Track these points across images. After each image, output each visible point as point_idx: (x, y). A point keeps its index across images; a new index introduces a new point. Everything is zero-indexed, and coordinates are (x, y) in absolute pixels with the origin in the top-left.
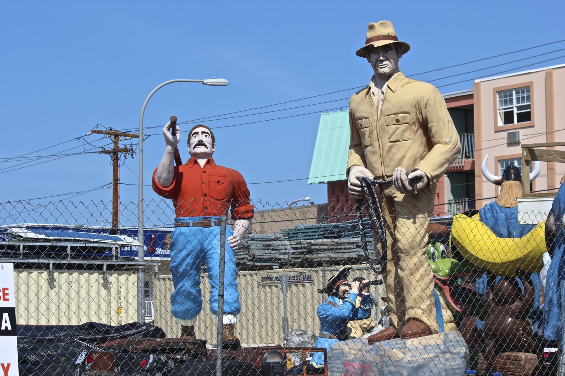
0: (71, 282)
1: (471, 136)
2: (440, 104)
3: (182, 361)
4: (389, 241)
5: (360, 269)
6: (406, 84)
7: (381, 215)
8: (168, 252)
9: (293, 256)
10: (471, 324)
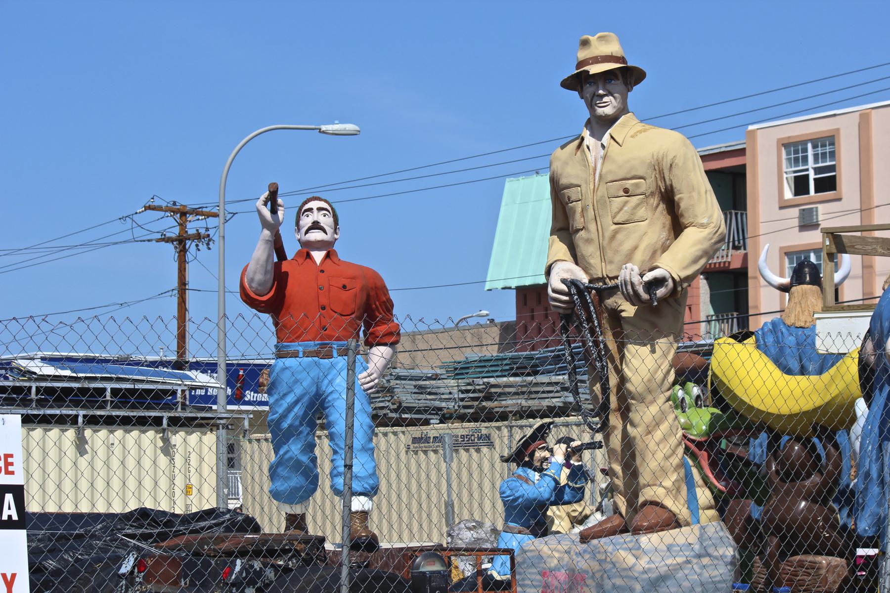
0: (113, 444)
1: (742, 215)
2: (694, 164)
3: (287, 570)
4: (613, 380)
5: (567, 425)
6: (640, 132)
7: (601, 338)
8: (265, 397)
9: (461, 403)
10: (742, 510)
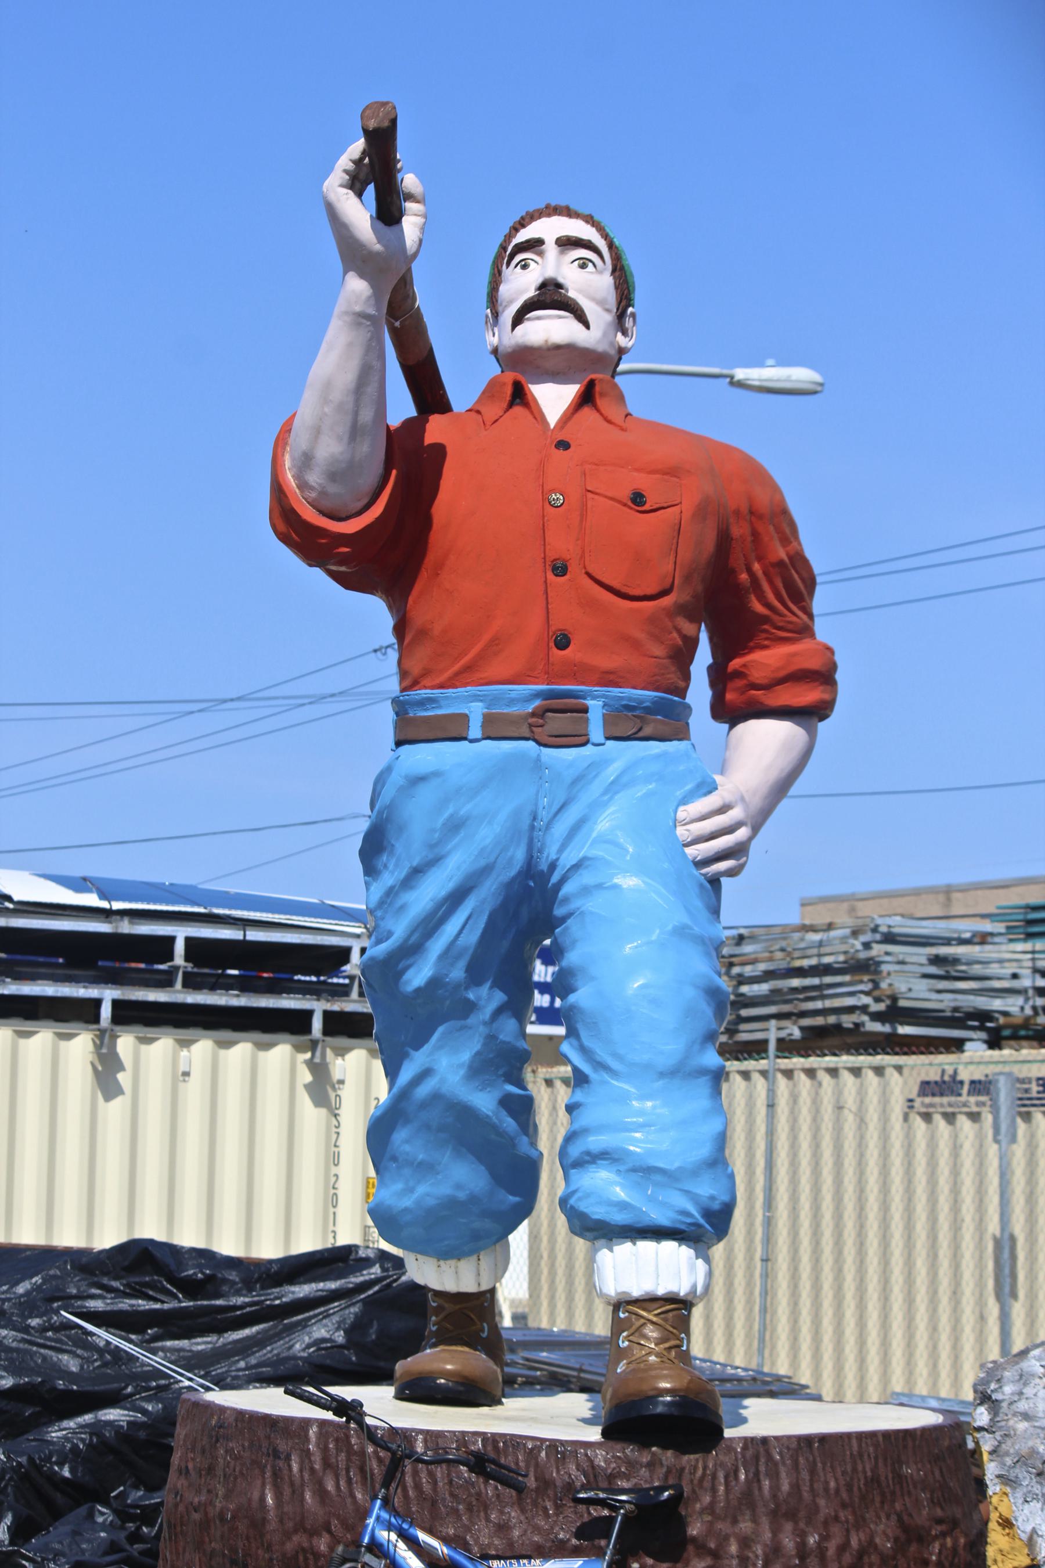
0: (186, 1074)
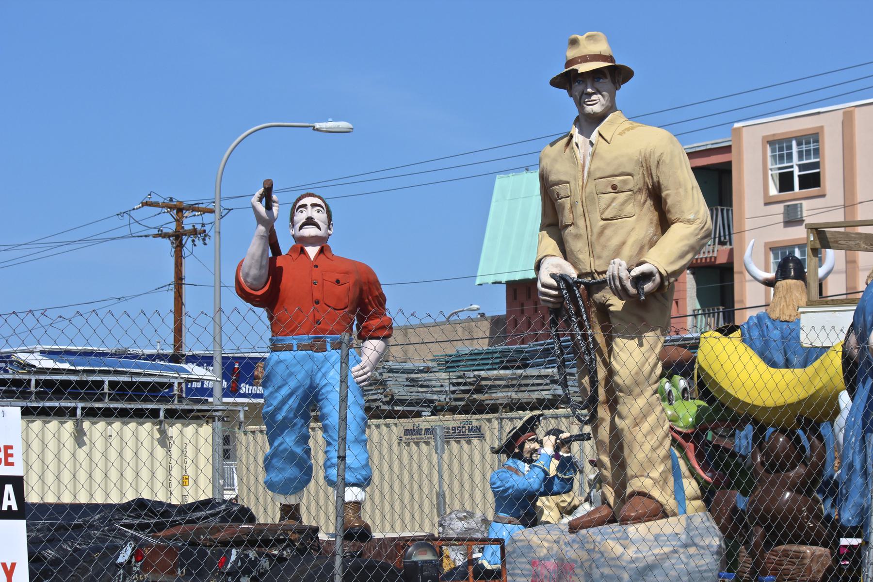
0: (110, 436)
1: (728, 211)
2: (681, 161)
3: (281, 559)
4: (602, 373)
5: (556, 417)
6: (628, 129)
7: (589, 332)
8: (260, 390)
9: (452, 396)
10: (728, 501)
